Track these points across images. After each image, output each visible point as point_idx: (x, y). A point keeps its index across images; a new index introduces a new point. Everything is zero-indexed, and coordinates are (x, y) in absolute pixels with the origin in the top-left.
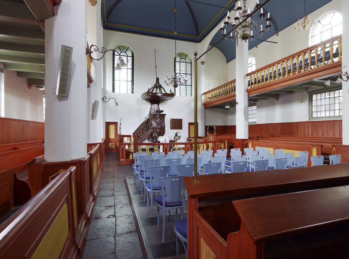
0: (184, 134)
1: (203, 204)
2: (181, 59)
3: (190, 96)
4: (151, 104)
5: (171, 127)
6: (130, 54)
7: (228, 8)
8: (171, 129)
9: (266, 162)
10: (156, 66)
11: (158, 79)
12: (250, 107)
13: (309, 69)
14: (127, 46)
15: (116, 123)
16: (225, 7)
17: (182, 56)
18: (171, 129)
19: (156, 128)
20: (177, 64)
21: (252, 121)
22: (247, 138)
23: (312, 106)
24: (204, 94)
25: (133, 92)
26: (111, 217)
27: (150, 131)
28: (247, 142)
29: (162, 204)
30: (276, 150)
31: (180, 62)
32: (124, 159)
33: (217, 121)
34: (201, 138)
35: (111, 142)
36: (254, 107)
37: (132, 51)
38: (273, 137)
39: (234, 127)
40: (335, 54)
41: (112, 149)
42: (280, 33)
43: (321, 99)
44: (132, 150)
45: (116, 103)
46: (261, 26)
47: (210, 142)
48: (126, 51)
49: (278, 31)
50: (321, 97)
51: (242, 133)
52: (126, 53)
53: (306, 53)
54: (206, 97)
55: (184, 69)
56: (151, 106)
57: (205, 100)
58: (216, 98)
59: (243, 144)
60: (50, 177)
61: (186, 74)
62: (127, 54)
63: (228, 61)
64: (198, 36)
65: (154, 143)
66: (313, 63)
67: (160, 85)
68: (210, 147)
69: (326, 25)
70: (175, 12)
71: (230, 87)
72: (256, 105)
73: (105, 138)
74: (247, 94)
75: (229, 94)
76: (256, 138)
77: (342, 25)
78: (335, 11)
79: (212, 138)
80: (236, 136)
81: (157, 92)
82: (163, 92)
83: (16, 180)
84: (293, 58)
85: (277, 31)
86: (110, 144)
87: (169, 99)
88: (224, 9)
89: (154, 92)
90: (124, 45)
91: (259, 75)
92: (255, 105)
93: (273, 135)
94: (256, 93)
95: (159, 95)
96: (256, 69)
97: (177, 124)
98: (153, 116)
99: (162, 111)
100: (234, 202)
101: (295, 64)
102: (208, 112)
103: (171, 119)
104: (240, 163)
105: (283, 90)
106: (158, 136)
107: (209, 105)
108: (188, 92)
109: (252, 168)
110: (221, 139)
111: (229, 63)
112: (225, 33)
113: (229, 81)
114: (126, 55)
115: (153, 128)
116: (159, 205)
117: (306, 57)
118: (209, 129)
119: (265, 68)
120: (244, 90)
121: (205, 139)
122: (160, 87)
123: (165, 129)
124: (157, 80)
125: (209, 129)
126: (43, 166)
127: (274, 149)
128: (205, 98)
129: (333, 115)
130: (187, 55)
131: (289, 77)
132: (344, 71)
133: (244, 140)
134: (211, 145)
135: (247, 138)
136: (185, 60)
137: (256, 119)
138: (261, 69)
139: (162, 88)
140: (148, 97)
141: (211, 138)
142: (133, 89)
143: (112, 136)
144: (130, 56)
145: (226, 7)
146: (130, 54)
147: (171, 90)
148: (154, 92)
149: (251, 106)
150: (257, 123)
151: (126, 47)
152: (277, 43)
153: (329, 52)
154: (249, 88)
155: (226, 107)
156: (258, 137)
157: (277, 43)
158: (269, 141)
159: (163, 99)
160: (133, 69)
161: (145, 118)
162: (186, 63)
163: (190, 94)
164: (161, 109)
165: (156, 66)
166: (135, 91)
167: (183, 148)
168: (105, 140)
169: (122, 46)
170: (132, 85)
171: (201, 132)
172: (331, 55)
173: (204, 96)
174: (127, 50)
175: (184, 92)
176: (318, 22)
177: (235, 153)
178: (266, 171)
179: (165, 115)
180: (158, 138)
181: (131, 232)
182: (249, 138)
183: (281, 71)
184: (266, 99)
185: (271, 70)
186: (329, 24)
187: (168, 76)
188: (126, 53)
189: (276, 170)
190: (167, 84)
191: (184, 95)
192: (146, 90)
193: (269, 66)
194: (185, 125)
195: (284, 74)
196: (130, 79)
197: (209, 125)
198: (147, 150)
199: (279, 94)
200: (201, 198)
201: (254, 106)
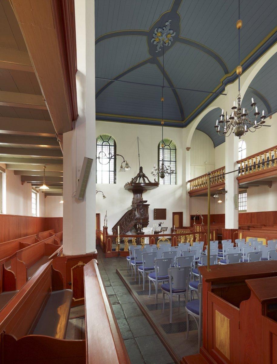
0: (168, 223)
1: (215, 287)
3: (174, 184)
4: (134, 194)
5: (154, 218)
6: (112, 144)
7: (217, 92)
8: (154, 219)
9: (258, 254)
10: (139, 154)
11: (141, 169)
12: (240, 195)
14: (110, 135)
16: (213, 92)
17: (166, 143)
18: (154, 219)
19: (139, 219)
20: (161, 151)
21: (242, 210)
22: (237, 228)
25: (115, 183)
26: (116, 304)
27: (133, 223)
28: (237, 232)
29: (169, 291)
30: (268, 242)
32: (110, 251)
33: (201, 210)
34: (186, 228)
36: (245, 195)
37: (114, 140)
38: (265, 226)
42: (273, 116)
44: (118, 242)
45: (104, 196)
47: (197, 233)
48: (108, 141)
49: (272, 113)
51: (231, 223)
52: (109, 143)
54: (192, 185)
55: (168, 156)
56: (134, 196)
57: (191, 188)
58: (202, 186)
59: (233, 235)
60: (71, 268)
61: (170, 161)
62: (109, 144)
63: (215, 146)
64: (183, 121)
65: (138, 234)
67: (144, 174)
70: (162, 101)
72: (246, 192)
74: (237, 181)
75: (218, 182)
76: (247, 228)
79: (199, 229)
80: (225, 226)
81: (140, 182)
82: (147, 182)
83: (4, 270)
85: (271, 114)
87: (152, 189)
88: (211, 94)
89: (137, 182)
90: (107, 134)
91: (251, 162)
92: (245, 192)
93: (265, 225)
94: (246, 181)
95: (142, 185)
96: (247, 155)
97: (160, 214)
98: (136, 207)
99: (146, 201)
100: (246, 280)
102: (194, 200)
103: (155, 209)
104: (235, 255)
106: (142, 228)
109: (244, 259)
111: (216, 148)
112: (219, 129)
113: (216, 168)
114: (108, 145)
115: (137, 219)
116: (167, 292)
118: (195, 219)
119: (257, 155)
120: (234, 178)
121: (192, 229)
122: (144, 176)
124: (140, 169)
125: (195, 219)
126: (67, 259)
127: (267, 240)
128: (190, 186)
130: (172, 141)
133: (233, 231)
134: (197, 236)
135: (237, 228)
136: (169, 147)
137: (246, 207)
138: (253, 156)
139: (146, 177)
140: (131, 187)
141: (198, 228)
142: (115, 179)
145: (214, 91)
148: (137, 182)
149: (241, 193)
150: (248, 212)
151: (108, 136)
152: (270, 126)
154: (239, 175)
155: (214, 196)
156: (249, 227)
157: (270, 126)
158: (261, 231)
159: (147, 188)
161: (128, 209)
162: (170, 149)
163: (174, 182)
164: (144, 200)
165: (139, 154)
166: (117, 181)
167: (169, 239)
169: (104, 136)
170: (114, 175)
171: (186, 222)
173: (189, 183)
174: (109, 139)
175: (168, 182)
177: (227, 244)
178: (260, 262)
179: (149, 205)
180: (142, 229)
181: (139, 316)
182: (239, 228)
184: (258, 186)
185: (263, 156)
187: (155, 166)
188: (109, 143)
189: (269, 261)
190: (154, 174)
192: (130, 181)
193: (262, 153)
194: (169, 216)
196: (112, 169)
198: (133, 242)
199: (272, 181)
200: (213, 282)
201: (244, 194)
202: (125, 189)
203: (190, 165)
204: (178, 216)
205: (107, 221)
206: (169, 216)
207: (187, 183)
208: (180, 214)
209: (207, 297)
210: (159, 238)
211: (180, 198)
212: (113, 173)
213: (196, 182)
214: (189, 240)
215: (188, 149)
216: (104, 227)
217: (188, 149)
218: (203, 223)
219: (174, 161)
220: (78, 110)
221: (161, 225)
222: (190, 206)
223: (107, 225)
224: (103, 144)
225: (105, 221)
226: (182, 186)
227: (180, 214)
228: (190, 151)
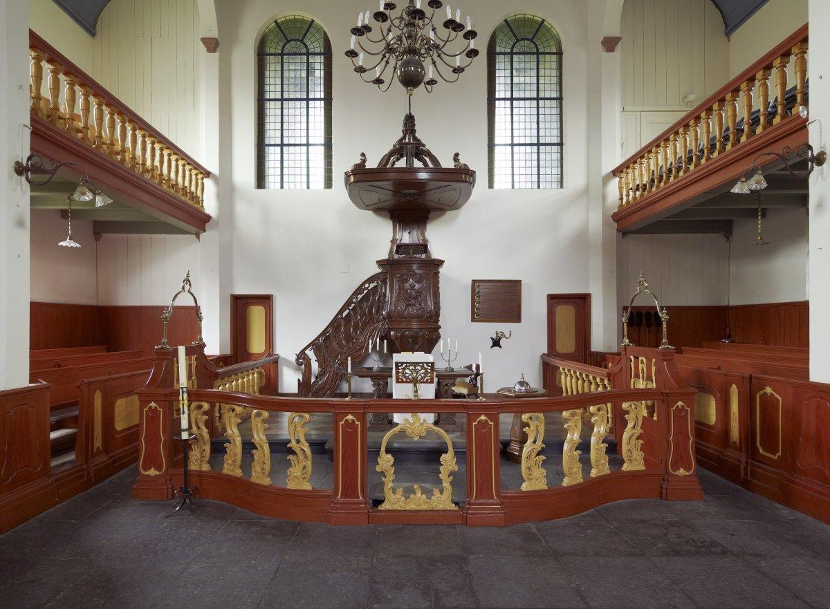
3: (555, 185)
6: (317, 47)
8: (473, 320)
11: (410, 121)
15: (266, 301)
18: (473, 320)
24: (617, 172)
32: (159, 468)
37: (325, 34)
39: (799, 312)
46: (654, 360)
47: (639, 395)
54: (627, 184)
57: (621, 199)
61: (538, 99)
68: (630, 425)
71: (758, 105)
102: (638, 247)
107: (636, 220)
108: (548, 171)
110: (663, 176)
114: (304, 51)
122: (419, 151)
123: (437, 321)
128: (621, 188)
144: (317, 50)
146: (316, 44)
147: (457, 155)
160: (328, 100)
163: (556, 178)
191: (529, 185)
194: (534, 307)
197: (169, 303)
203: (618, 108)
206: (534, 307)
207: (606, 180)
208: (581, 302)
209: (738, 21)
210: (397, 418)
211: (580, 241)
214: (573, 436)
215: (610, 44)
217: (610, 44)
218: (665, 345)
219: (555, 96)
222: (621, 274)
224: (286, 51)
226: (586, 191)
227: (581, 302)
228: (617, 54)
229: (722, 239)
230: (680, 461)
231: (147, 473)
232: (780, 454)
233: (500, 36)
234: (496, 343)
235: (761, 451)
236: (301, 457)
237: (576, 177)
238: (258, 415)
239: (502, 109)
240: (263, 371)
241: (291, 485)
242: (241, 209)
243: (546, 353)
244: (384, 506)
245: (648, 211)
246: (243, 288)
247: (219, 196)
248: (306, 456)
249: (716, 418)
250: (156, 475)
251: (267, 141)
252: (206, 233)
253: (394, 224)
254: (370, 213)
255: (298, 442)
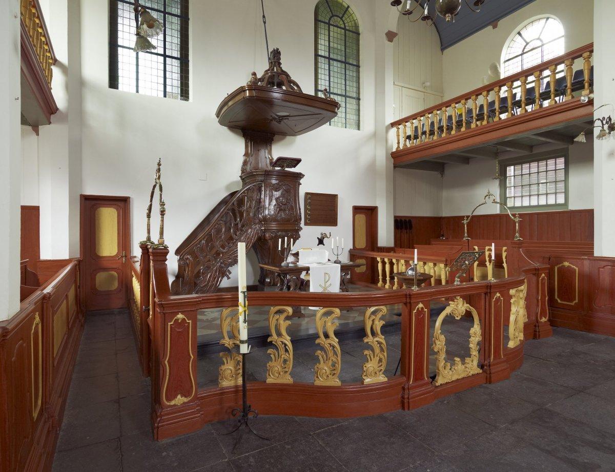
2: (333, 16)
11: (275, 57)
13: (496, 119)
15: (122, 204)
23: (505, 188)
24: (393, 125)
31: (329, 24)
35: (105, 269)
40: (543, 93)
41: (108, 294)
43: (538, 172)
50: (546, 167)
53: (479, 97)
66: (504, 109)
69: (531, 41)
73: (77, 255)
77: (563, 39)
78: (547, 15)
84: (477, 95)
86: (101, 277)
101: (493, 103)
105: (435, 160)
111: (446, 51)
115: (265, 219)
117: (490, 99)
129: (544, 203)
130: (348, 7)
131: (460, 133)
132: (599, 113)
136: (341, 22)
143: (109, 247)
153: (533, 89)
161: (228, 187)
168: (76, 265)
171: (385, 234)
172: (537, 95)
173: (394, 129)
176: (518, 35)
183: (444, 123)
186: (539, 39)
194: (345, 214)
195: (449, 128)
202: (222, 123)
204: (364, 216)
205: (163, 213)
211: (371, 169)
212: (176, 63)
213: (401, 131)
216: (144, 247)
217: (391, 36)
220: (117, 228)
221: (325, 241)
222: (395, 195)
223: (162, 233)
225: (149, 216)
226: (374, 135)
229: (439, 176)
230: (543, 314)
231: (173, 403)
232: (577, 301)
233: (321, 9)
234: (321, 242)
235: (559, 301)
236: (282, 351)
237: (368, 123)
238: (279, 312)
239: (323, 64)
240: (116, 273)
241: (320, 382)
242: (91, 106)
243: (352, 248)
244: (440, 381)
245: (428, 152)
246: (90, 191)
247: (67, 87)
248: (335, 353)
249: (118, 284)
250: (184, 403)
251: (120, 42)
252: (51, 125)
253: (246, 141)
254: (225, 128)
255: (327, 336)
